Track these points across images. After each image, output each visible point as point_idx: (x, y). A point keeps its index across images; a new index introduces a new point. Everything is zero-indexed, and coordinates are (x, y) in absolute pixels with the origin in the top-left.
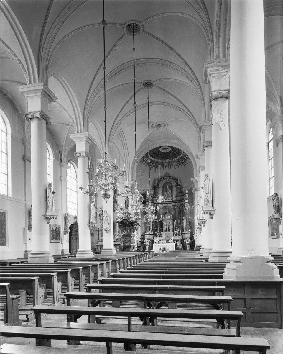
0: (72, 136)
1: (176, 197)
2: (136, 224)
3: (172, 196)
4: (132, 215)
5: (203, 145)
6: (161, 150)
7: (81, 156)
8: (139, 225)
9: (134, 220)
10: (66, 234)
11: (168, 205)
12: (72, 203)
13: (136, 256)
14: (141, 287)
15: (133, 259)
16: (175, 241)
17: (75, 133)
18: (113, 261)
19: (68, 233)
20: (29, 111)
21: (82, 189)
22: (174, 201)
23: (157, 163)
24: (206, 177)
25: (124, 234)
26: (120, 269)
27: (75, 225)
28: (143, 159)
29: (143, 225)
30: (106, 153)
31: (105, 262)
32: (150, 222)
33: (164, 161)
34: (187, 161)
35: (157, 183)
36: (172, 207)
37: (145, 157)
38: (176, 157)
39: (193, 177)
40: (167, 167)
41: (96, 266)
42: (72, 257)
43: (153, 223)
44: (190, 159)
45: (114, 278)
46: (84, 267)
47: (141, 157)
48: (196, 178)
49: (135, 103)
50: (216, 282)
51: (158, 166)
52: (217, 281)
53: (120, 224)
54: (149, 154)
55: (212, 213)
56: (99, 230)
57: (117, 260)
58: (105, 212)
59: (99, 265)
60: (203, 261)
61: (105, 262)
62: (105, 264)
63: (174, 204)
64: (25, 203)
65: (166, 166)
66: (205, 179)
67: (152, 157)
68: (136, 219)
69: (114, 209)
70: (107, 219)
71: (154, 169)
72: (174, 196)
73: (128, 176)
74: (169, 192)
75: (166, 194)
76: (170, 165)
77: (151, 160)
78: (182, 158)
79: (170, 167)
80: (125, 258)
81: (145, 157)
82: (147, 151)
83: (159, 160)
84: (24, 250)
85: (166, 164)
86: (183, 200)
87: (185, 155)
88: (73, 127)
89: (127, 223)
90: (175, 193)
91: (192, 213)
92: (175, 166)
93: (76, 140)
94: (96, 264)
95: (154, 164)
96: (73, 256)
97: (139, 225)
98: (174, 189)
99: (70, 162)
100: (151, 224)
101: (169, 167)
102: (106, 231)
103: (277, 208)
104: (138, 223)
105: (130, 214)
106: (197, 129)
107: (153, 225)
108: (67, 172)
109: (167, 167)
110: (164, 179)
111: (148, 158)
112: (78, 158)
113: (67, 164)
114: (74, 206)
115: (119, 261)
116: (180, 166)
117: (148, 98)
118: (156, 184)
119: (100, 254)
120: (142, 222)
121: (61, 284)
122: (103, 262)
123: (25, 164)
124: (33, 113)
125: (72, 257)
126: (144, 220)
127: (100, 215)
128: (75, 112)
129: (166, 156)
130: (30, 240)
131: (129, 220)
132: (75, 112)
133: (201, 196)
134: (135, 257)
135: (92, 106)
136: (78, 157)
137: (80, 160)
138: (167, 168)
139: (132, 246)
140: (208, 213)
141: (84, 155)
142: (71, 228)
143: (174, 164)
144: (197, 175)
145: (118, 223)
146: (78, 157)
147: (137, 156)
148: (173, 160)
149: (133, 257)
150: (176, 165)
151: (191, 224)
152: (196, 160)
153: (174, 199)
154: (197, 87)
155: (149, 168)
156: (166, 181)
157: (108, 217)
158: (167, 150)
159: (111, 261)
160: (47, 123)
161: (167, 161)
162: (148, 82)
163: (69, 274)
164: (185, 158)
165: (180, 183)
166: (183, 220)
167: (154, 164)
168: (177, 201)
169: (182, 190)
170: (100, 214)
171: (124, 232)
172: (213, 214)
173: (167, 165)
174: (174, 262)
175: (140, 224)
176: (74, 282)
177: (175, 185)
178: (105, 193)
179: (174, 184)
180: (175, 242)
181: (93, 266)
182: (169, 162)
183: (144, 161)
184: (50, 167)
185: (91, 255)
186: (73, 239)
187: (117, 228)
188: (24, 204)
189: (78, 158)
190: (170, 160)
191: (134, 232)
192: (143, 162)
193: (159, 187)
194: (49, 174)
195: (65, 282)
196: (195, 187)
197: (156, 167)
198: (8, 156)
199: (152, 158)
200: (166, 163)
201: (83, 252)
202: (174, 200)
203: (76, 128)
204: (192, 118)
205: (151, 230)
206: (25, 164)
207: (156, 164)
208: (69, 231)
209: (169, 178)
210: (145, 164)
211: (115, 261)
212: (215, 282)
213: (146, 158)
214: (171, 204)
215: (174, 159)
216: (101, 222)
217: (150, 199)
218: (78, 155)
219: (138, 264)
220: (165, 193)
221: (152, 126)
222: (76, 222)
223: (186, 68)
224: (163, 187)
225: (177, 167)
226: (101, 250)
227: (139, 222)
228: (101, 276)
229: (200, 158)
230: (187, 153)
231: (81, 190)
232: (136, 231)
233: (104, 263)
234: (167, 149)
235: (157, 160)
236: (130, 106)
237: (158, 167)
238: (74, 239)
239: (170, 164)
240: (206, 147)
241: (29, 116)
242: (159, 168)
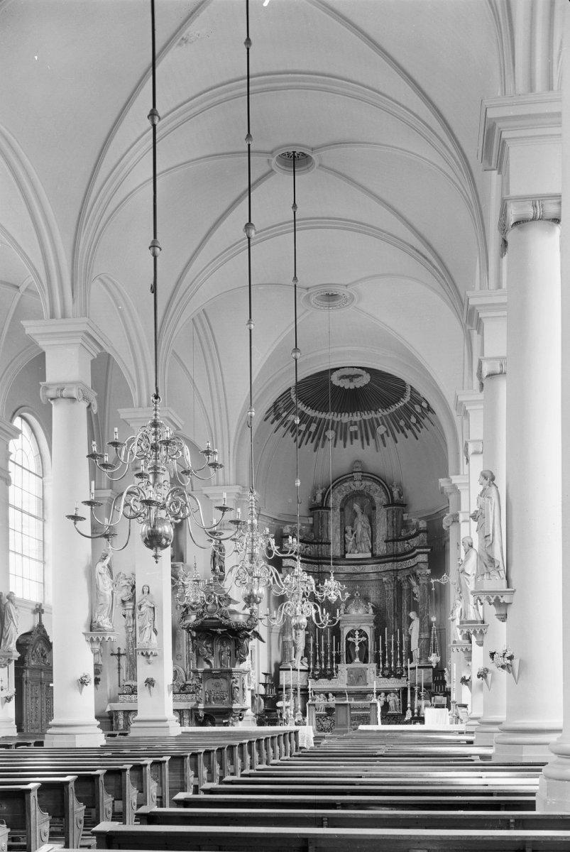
0: (31, 327)
1: (386, 541)
2: (250, 633)
3: (373, 539)
4: (236, 603)
5: (504, 213)
6: (335, 379)
7: (62, 397)
8: (261, 639)
9: (241, 619)
10: (5, 665)
11: (358, 569)
12: (20, 552)
13: (250, 743)
14: (282, 834)
15: (242, 753)
16: (383, 694)
17: (42, 318)
18: (173, 758)
19: (12, 665)
21: (79, 522)
22: (380, 557)
23: (323, 426)
24: (486, 482)
25: (208, 667)
26: (242, 770)
27: (36, 637)
28: (275, 409)
29: (275, 638)
30: (157, 397)
31: (149, 761)
32: (297, 627)
33: (345, 418)
34: (426, 419)
35: (323, 495)
36: (373, 577)
37: (281, 404)
38: (386, 407)
39: (446, 475)
40: (356, 438)
41: (119, 773)
42: (28, 744)
43: (306, 630)
44: (433, 412)
45: (185, 807)
46: (44, 784)
47: (268, 403)
48: (455, 480)
50: (512, 821)
51: (325, 437)
52: (512, 816)
53: (194, 634)
54: (299, 397)
55: (505, 599)
56: (119, 655)
57: (189, 754)
58: (146, 591)
59: (128, 772)
60: (472, 758)
61: (149, 761)
62: (148, 767)
63: (381, 567)
65: (354, 435)
66: (481, 488)
67: (307, 405)
68: (251, 616)
69: (173, 582)
70: (150, 614)
71: (311, 446)
72: (380, 539)
74: (361, 524)
75: (352, 532)
76: (367, 431)
77: (302, 415)
78: (407, 410)
79: (368, 439)
80: (237, 743)
81: (281, 404)
82: (291, 382)
83: (329, 416)
85: (353, 429)
86: (410, 555)
87: (417, 399)
88: (37, 294)
89: (219, 631)
90: (382, 530)
91: (438, 596)
92: (382, 436)
93: (47, 343)
94: (120, 767)
95: (313, 427)
96: (32, 741)
97: (261, 639)
98: (382, 515)
99: (21, 416)
100: (302, 634)
101: (362, 440)
102: (148, 656)
104: (256, 629)
105: (230, 599)
106: (460, 315)
107: (307, 637)
108: (11, 449)
109: (355, 441)
110: (345, 481)
111: (290, 407)
113: (11, 420)
114: (33, 569)
115: (193, 759)
116: (400, 436)
117: (295, 206)
118: (319, 497)
119: (125, 735)
120: (270, 628)
121: (9, 830)
122: (210, 749)
125: (28, 744)
126: (277, 624)
127: (123, 602)
128: (42, 246)
129: (352, 400)
130: (2, 690)
131: (225, 622)
132: (42, 246)
133: (470, 541)
134: (214, 757)
135: (100, 226)
136: (52, 399)
137: (58, 411)
138: (357, 442)
139: (237, 709)
140: (492, 601)
142: (20, 646)
143: (381, 430)
144: (458, 466)
145: (188, 629)
146: (52, 399)
147: (257, 397)
148: (379, 415)
149: (241, 745)
150: (387, 432)
151: (436, 640)
152: (457, 420)
153: (381, 549)
154: (459, 173)
155: (296, 440)
156: (353, 487)
157: (154, 608)
158: (355, 380)
159: (169, 758)
161: (356, 417)
162: (294, 152)
163: (33, 798)
164: (418, 408)
165: (400, 494)
166: (410, 621)
167: (313, 427)
168: (391, 556)
169: (405, 519)
170: (124, 599)
171: (209, 662)
172: (508, 604)
173: (356, 432)
174: (378, 762)
175: (264, 636)
176: (48, 824)
177: (385, 503)
178: (152, 531)
179: (380, 498)
180: (383, 699)
181: (110, 773)
182: (365, 421)
183: (277, 418)
185: (97, 738)
186: (29, 686)
187: (185, 649)
189: (52, 402)
190: (367, 416)
191: (242, 661)
192: (276, 423)
193: (329, 509)
195: (92, 804)
196: (452, 510)
197: (318, 437)
199: (304, 409)
200: (351, 425)
202: (378, 552)
203: (47, 301)
204: (442, 277)
205: (300, 654)
207: (317, 428)
208: (16, 655)
209: (364, 478)
210: (282, 429)
211: (182, 758)
213: (286, 409)
214: (368, 568)
215: (382, 413)
216: (127, 628)
217: (299, 551)
218: (51, 393)
219: (283, 758)
220: (349, 529)
221: (308, 297)
222: (41, 626)
224: (342, 510)
225: (389, 440)
226: (127, 725)
227: (261, 629)
228: (46, 839)
229: (471, 414)
230: (424, 392)
231: (75, 523)
232: (248, 658)
233: (146, 765)
234: (358, 376)
235: (322, 415)
236: (233, 227)
237: (324, 440)
238: (32, 686)
239: (366, 431)
240: (516, 229)
242: (330, 444)
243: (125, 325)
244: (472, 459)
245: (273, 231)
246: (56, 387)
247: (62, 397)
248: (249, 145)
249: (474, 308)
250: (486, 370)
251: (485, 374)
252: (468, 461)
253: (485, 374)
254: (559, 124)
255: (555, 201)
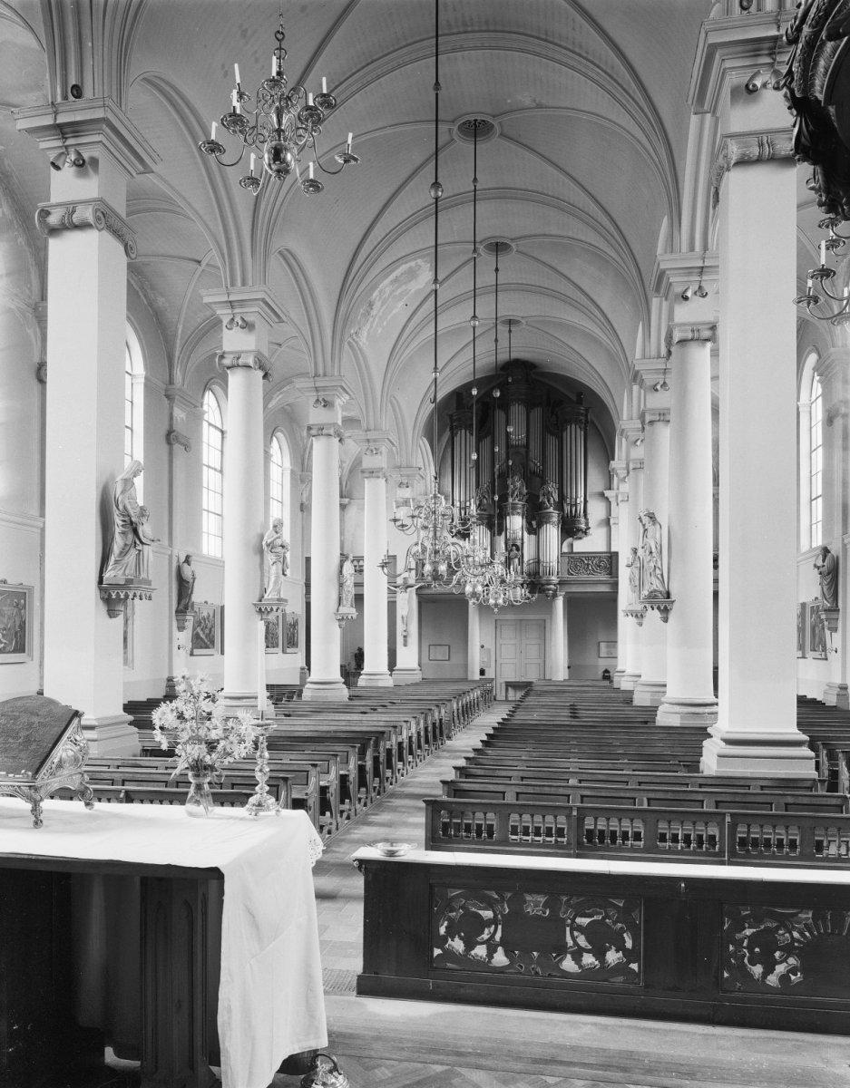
12: (210, 514)
20: (55, 198)
49: (436, 185)
64: (42, 525)
73: (79, 24)
84: (166, 676)
88: (219, 269)
103: (831, 574)
112: (228, 372)
123: (171, 454)
124: (71, 207)
136: (228, 368)
141: (251, 361)
146: (228, 368)
160: (265, 376)
184: (282, 485)
188: (167, 557)
189: (228, 372)
194: (128, 424)
198: (134, 435)
201: (372, 677)
206: (171, 454)
212: (733, 854)
218: (227, 362)
223: (597, 313)
236: (419, 196)
241: (53, 220)
243: (304, 303)
244: (620, 504)
245: (457, 200)
246: (232, 356)
247: (238, 366)
248: (437, 94)
249: (638, 372)
250: (677, 336)
251: (676, 339)
252: (618, 504)
253: (676, 339)
254: (717, 273)
255: (788, 136)
